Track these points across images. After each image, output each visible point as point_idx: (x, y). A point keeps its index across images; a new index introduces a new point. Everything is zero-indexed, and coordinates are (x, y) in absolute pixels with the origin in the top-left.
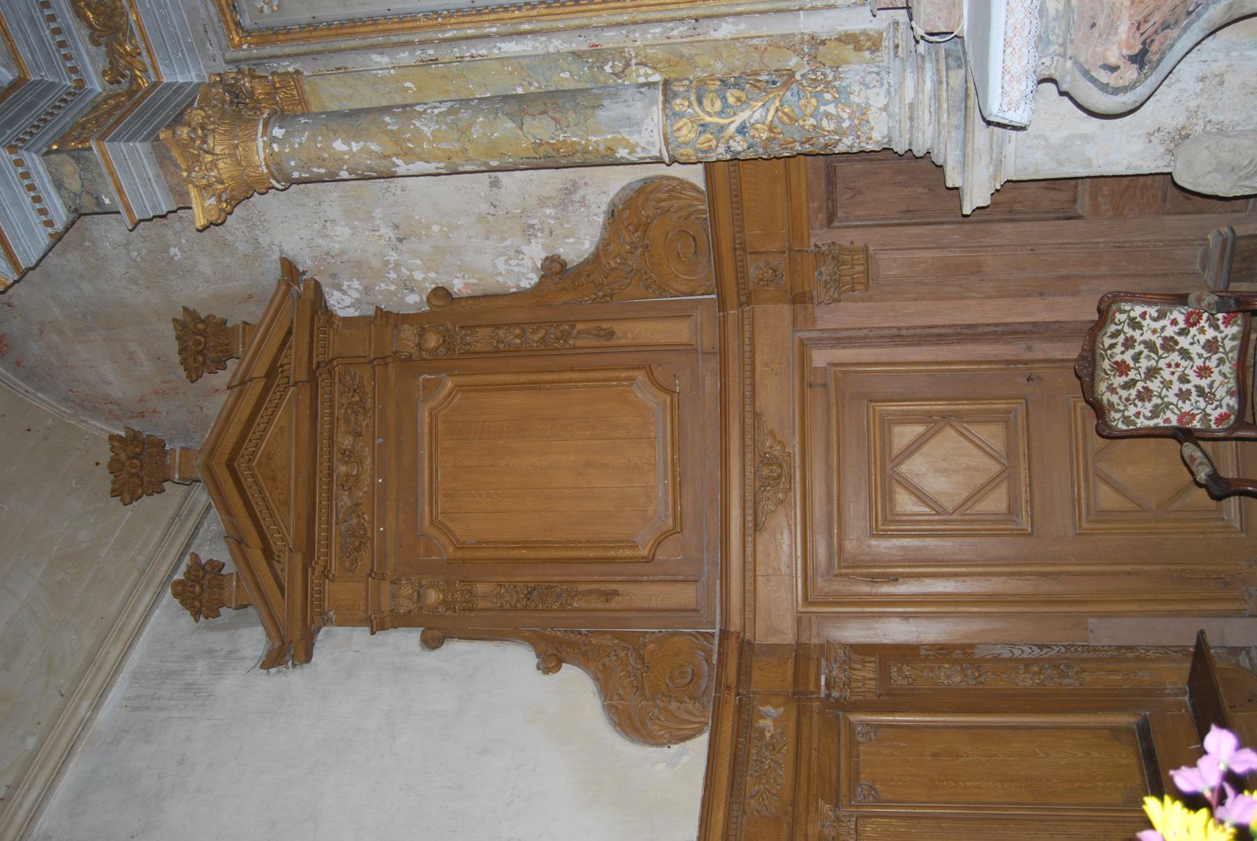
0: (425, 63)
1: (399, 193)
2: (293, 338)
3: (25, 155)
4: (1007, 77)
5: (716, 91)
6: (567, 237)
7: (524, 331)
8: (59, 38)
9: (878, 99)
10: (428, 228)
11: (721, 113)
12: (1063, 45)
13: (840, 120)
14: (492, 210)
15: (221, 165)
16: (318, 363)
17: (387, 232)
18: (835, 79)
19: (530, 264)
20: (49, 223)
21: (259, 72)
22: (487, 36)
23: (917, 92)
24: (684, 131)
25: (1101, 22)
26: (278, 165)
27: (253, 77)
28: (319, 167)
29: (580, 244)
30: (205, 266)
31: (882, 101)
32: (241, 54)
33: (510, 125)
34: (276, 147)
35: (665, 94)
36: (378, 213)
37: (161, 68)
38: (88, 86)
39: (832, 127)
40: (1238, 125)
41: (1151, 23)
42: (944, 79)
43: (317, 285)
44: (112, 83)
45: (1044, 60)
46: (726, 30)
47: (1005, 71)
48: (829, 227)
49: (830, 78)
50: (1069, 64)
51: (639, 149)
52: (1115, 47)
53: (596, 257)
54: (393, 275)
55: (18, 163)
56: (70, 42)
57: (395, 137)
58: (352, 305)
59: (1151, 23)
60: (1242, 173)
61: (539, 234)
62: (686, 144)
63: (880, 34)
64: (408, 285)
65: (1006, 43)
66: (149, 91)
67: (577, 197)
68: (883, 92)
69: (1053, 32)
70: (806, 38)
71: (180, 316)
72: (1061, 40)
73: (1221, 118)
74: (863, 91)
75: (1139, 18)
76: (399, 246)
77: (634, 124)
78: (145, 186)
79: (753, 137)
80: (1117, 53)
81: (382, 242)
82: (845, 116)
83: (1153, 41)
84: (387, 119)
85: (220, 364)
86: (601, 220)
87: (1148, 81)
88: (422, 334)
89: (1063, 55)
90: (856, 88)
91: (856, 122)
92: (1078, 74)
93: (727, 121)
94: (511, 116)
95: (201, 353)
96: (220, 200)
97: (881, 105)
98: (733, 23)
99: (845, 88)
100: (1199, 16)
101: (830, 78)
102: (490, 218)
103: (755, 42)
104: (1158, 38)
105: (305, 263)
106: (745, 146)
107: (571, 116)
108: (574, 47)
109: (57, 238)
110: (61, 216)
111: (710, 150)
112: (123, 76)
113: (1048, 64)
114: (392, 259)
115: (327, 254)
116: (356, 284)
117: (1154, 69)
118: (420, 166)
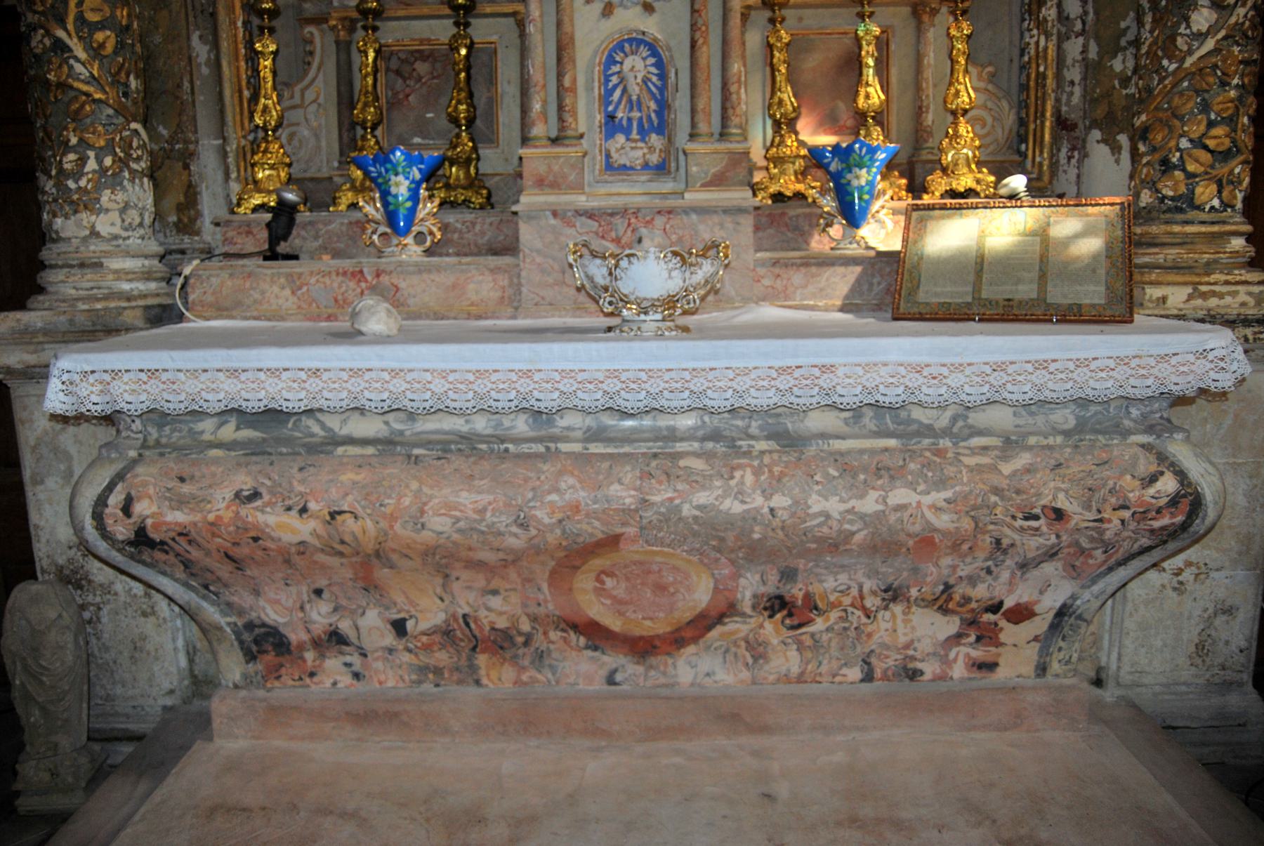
4: (107, 377)
5: (113, 16)
11: (80, 19)
12: (158, 443)
13: (77, 174)
18: (132, 171)
23: (116, 272)
25: (186, 489)
40: (98, 639)
41: (188, 548)
42: (134, 304)
45: (138, 422)
47: (115, 373)
49: (134, 166)
50: (133, 454)
52: (154, 509)
59: (188, 548)
60: (30, 661)
63: (198, 233)
65: (153, 373)
68: (116, 230)
69: (173, 431)
70: (192, 147)
72: (164, 440)
73: (104, 620)
74: (115, 206)
75: (193, 534)
79: (50, 62)
80: (147, 512)
82: (83, 183)
83: (167, 553)
89: (144, 446)
90: (120, 197)
91: (75, 197)
92: (117, 467)
93: (70, 27)
97: (98, 228)
98: (209, 58)
99: (121, 184)
100: (204, 597)
101: (134, 166)
103: (186, 85)
104: (171, 558)
106: (38, 51)
113: (134, 427)
117: (132, 557)
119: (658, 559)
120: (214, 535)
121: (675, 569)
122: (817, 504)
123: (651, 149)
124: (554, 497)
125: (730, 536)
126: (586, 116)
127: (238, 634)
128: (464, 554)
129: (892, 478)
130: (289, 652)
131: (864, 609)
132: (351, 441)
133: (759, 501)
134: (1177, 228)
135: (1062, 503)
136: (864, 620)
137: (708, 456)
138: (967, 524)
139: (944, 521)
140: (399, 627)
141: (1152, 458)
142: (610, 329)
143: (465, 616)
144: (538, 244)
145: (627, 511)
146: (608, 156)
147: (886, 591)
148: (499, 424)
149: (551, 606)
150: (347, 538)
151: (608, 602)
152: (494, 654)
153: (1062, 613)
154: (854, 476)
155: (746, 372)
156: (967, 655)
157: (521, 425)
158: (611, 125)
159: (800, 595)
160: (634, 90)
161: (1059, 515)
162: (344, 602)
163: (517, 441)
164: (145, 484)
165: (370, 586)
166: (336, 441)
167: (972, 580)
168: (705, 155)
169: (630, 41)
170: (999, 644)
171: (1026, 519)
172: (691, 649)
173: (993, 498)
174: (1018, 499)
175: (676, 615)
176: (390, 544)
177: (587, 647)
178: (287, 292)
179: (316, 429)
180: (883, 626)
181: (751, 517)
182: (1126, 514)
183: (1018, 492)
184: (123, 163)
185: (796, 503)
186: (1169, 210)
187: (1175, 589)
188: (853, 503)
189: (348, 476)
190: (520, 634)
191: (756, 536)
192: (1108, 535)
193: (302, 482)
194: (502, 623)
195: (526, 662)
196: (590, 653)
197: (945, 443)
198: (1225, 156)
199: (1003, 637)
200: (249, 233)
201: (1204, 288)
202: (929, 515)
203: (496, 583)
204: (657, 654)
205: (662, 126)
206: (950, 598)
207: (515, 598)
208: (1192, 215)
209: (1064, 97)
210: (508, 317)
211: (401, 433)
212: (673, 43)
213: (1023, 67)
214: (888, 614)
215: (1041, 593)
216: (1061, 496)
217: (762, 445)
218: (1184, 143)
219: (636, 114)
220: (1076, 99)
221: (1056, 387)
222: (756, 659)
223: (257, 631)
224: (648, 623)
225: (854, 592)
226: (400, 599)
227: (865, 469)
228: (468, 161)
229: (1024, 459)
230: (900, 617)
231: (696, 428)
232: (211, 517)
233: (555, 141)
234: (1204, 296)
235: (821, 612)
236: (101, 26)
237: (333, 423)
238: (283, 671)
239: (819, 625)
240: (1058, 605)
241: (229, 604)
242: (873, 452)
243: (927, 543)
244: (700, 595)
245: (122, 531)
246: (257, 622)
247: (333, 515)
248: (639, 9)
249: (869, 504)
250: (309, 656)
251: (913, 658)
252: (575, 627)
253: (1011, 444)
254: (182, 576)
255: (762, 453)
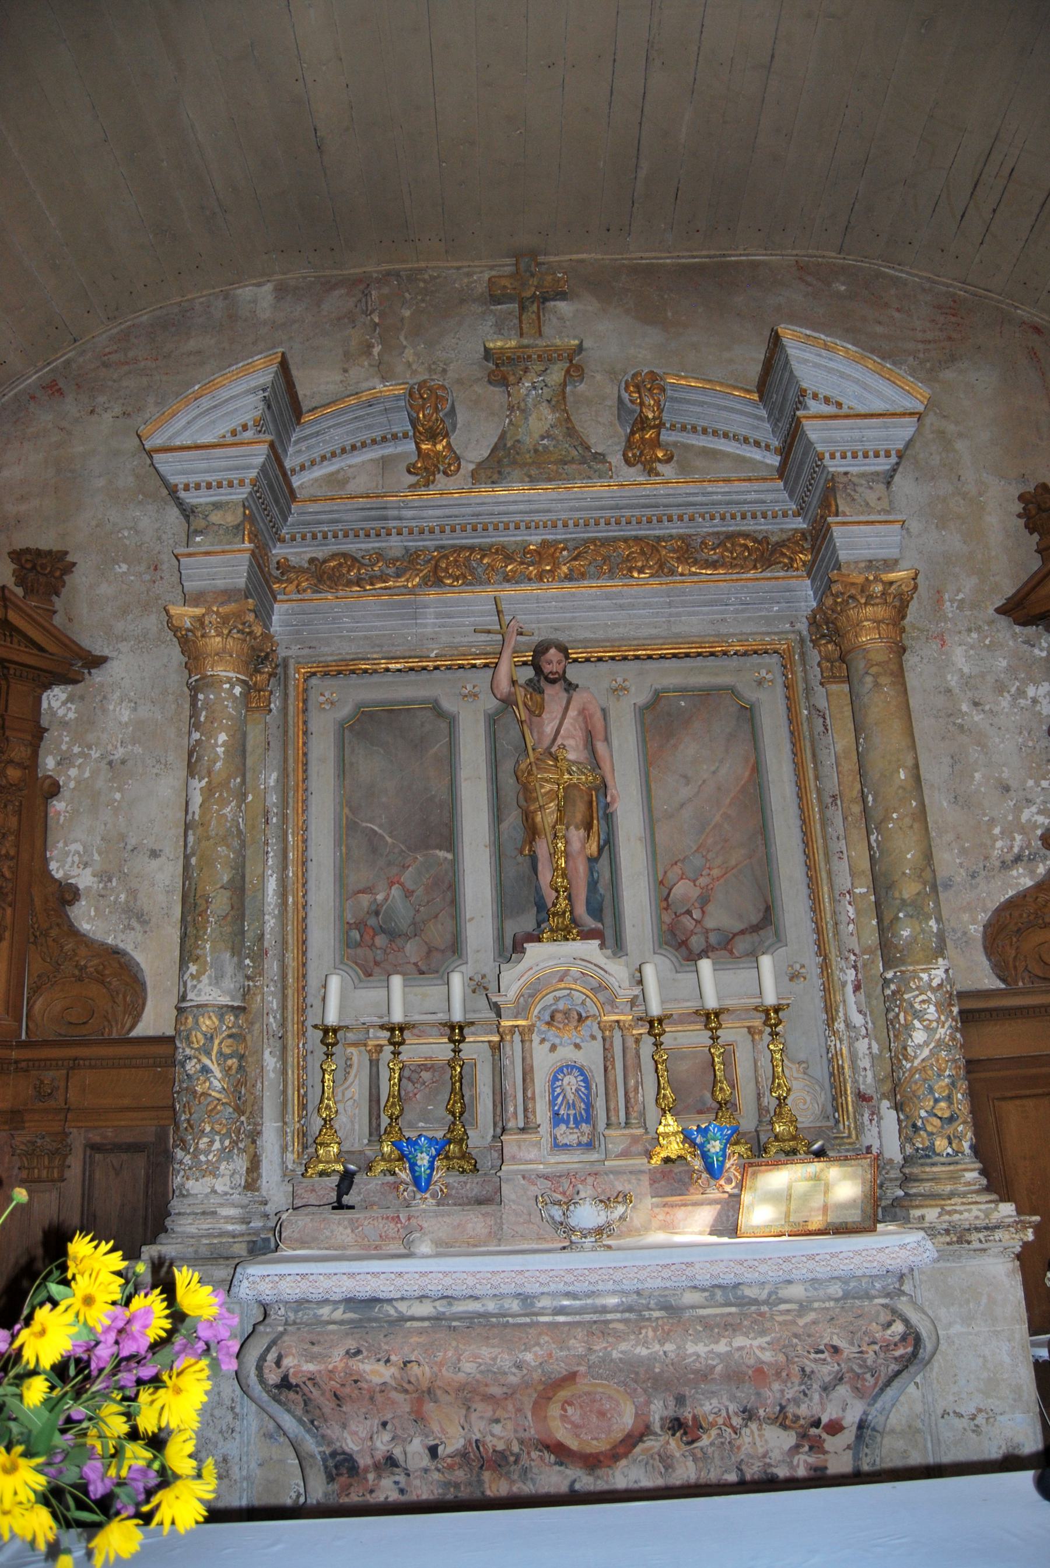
0: (266, 813)
1: (155, 771)
2: (35, 651)
3: (248, 489)
4: (277, 1279)
6: (97, 909)
7: (12, 858)
8: (320, 535)
9: (221, 1185)
10: (119, 789)
11: (220, 1053)
13: (207, 1153)
14: (129, 847)
15: (218, 639)
16: (8, 668)
17: (120, 753)
18: (239, 1149)
19: (72, 873)
20: (187, 488)
21: (272, 680)
22: (285, 868)
23: (226, 1217)
24: (208, 1022)
25: (316, 1349)
26: (211, 685)
27: (271, 675)
28: (206, 717)
29: (88, 920)
30: (105, 589)
31: (220, 1189)
32: (291, 671)
33: (226, 879)
34: (227, 686)
35: (238, 1008)
36: (138, 749)
37: (286, 606)
38: (278, 544)
39: (202, 1146)
43: (75, 682)
44: (278, 563)
46: (270, 1062)
47: (282, 1276)
48: (86, 1146)
49: (241, 1145)
50: (281, 1329)
51: (195, 982)
52: (296, 1362)
53: (74, 932)
54: (76, 750)
55: (242, 483)
56: (315, 543)
57: (225, 784)
58: (50, 707)
61: (101, 885)
62: (197, 1023)
64: (65, 761)
65: (303, 1276)
66: (270, 588)
67: (134, 923)
68: (227, 1189)
71: (70, 558)
76: (105, 762)
77: (217, 981)
78: (208, 574)
81: (110, 747)
82: (210, 1157)
84: (238, 780)
85: (21, 581)
86: (110, 941)
87: (264, 1394)
88: (20, 765)
89: (286, 1323)
94: (231, 881)
95: (34, 567)
96: (188, 630)
100: (308, 1431)
102: (122, 845)
103: (259, 1085)
105: (98, 676)
106: (191, 1072)
107: (228, 929)
108: (267, 936)
109: (173, 491)
110: (191, 498)
111: (190, 1044)
112: (282, 574)
114: (92, 752)
115: (105, 697)
116: (71, 715)
118: (197, 799)
119: (600, 1390)
120: (331, 1379)
121: (610, 1397)
122: (691, 1348)
123: (583, 1134)
124: (537, 1348)
125: (642, 1370)
126: (542, 1113)
127: (324, 1460)
128: (482, 1389)
129: (734, 1330)
130: (357, 1473)
131: (732, 1427)
132: (413, 1319)
133: (657, 1347)
134: (928, 1169)
135: (836, 1341)
136: (734, 1436)
137: (625, 1321)
138: (781, 1358)
139: (767, 1356)
140: (433, 1451)
141: (889, 1312)
142: (564, 1248)
143: (477, 1441)
144: (513, 1197)
145: (581, 1357)
146: (555, 1138)
147: (744, 1412)
148: (502, 1306)
149: (533, 1431)
150: (413, 1380)
151: (569, 1426)
152: (494, 1470)
153: (862, 1426)
154: (712, 1330)
155: (644, 1268)
156: (805, 1461)
157: (515, 1306)
158: (557, 1119)
159: (690, 1417)
160: (571, 1097)
161: (836, 1350)
162: (399, 1432)
163: (513, 1316)
164: (290, 1347)
165: (419, 1418)
166: (404, 1319)
167: (797, 1402)
168: (617, 1139)
169: (567, 1066)
170: (825, 1452)
171: (816, 1353)
172: (623, 1462)
173: (795, 1341)
174: (810, 1341)
175: (613, 1435)
176: (439, 1383)
177: (556, 1463)
178: (349, 1231)
179: (392, 1312)
180: (747, 1440)
181: (653, 1358)
182: (876, 1347)
183: (809, 1336)
184: (234, 1143)
185: (679, 1348)
186: (922, 1157)
187: (973, 1431)
188: (712, 1346)
189: (414, 1339)
190: (512, 1454)
191: (657, 1370)
192: (869, 1362)
193: (386, 1343)
194: (500, 1446)
195: (515, 1477)
196: (557, 1468)
197: (764, 1308)
198: (951, 1119)
199: (827, 1446)
200: (313, 1190)
201: (948, 1208)
202: (758, 1352)
203: (499, 1413)
204: (600, 1468)
205: (588, 1117)
206: (786, 1417)
207: (510, 1426)
208: (936, 1159)
209: (861, 1079)
210: (496, 1240)
211: (444, 1313)
212: (593, 1067)
213: (830, 1061)
214: (748, 1431)
215: (844, 1410)
216: (835, 1337)
217: (656, 1314)
218: (923, 1113)
219: (572, 1112)
220: (870, 1079)
221: (822, 1271)
222: (666, 1468)
223: (338, 1458)
224: (595, 1442)
225: (724, 1413)
226: (436, 1427)
227: (718, 1326)
228: (462, 1140)
229: (812, 1316)
230: (756, 1433)
231: (618, 1305)
232: (330, 1367)
233: (523, 1130)
234: (949, 1213)
235: (706, 1431)
236: (231, 1056)
237: (402, 1307)
238: (352, 1489)
239: (705, 1441)
240: (857, 1420)
241: (323, 1436)
242: (722, 1315)
243: (760, 1372)
244: (626, 1420)
245: (273, 1377)
246: (339, 1451)
247: (405, 1363)
248: (572, 1047)
249: (722, 1347)
250: (371, 1476)
251: (770, 1465)
252: (547, 1447)
253: (804, 1307)
254: (299, 1412)
255: (657, 1318)
